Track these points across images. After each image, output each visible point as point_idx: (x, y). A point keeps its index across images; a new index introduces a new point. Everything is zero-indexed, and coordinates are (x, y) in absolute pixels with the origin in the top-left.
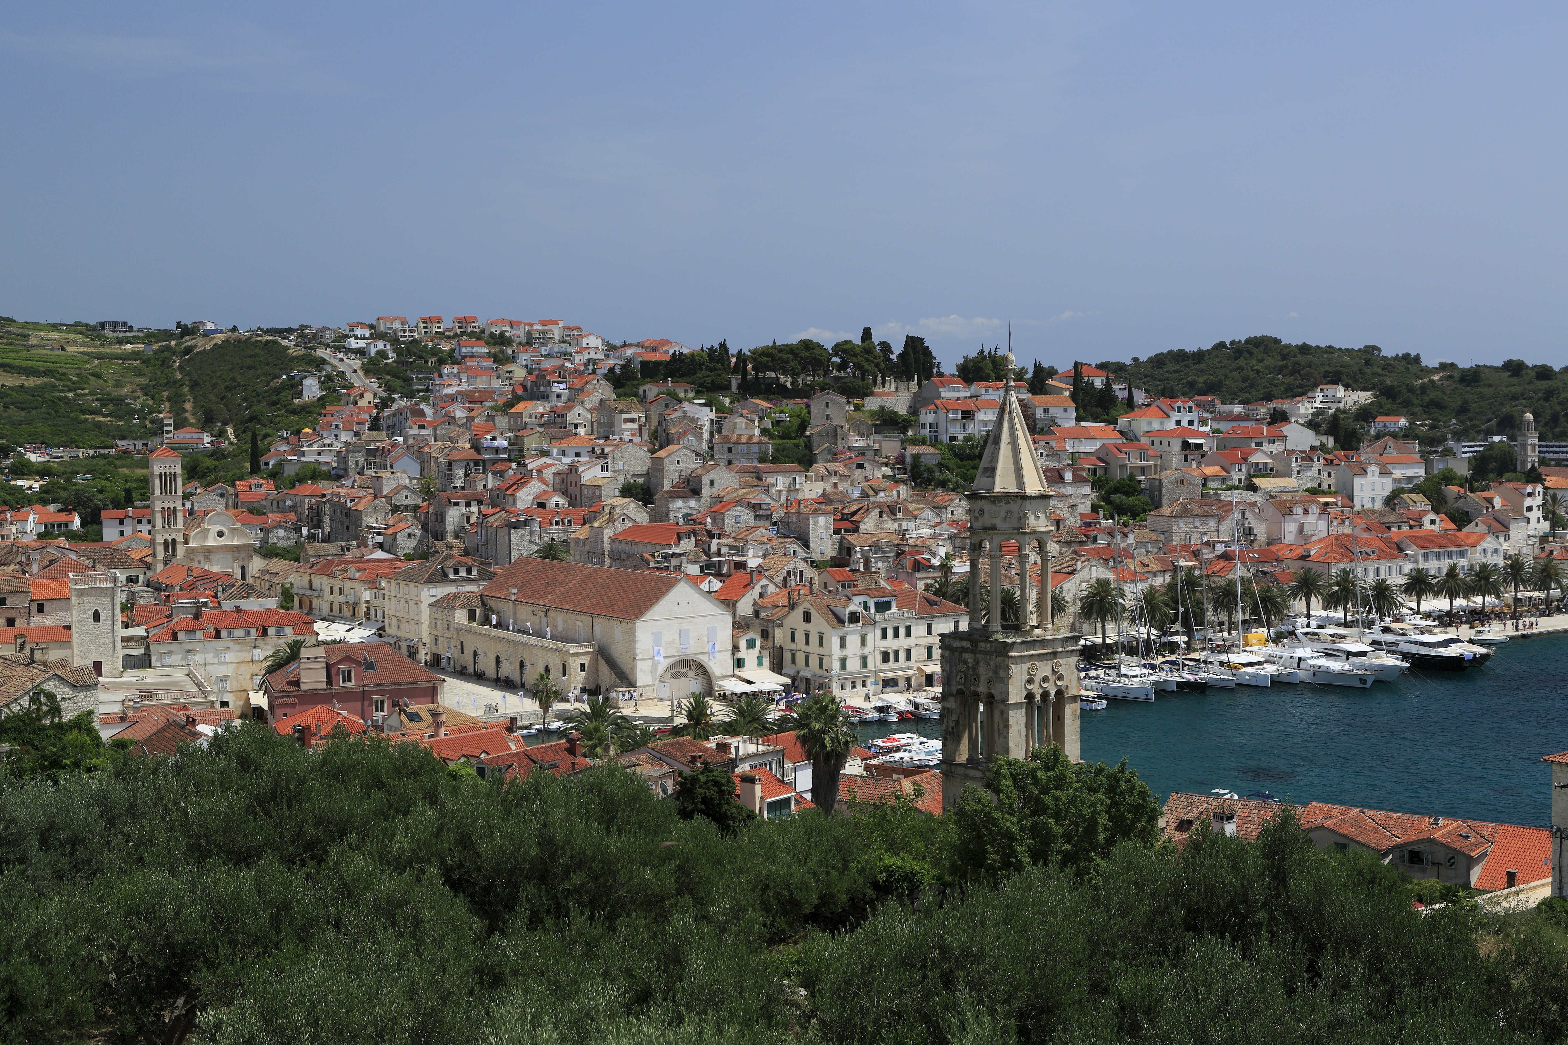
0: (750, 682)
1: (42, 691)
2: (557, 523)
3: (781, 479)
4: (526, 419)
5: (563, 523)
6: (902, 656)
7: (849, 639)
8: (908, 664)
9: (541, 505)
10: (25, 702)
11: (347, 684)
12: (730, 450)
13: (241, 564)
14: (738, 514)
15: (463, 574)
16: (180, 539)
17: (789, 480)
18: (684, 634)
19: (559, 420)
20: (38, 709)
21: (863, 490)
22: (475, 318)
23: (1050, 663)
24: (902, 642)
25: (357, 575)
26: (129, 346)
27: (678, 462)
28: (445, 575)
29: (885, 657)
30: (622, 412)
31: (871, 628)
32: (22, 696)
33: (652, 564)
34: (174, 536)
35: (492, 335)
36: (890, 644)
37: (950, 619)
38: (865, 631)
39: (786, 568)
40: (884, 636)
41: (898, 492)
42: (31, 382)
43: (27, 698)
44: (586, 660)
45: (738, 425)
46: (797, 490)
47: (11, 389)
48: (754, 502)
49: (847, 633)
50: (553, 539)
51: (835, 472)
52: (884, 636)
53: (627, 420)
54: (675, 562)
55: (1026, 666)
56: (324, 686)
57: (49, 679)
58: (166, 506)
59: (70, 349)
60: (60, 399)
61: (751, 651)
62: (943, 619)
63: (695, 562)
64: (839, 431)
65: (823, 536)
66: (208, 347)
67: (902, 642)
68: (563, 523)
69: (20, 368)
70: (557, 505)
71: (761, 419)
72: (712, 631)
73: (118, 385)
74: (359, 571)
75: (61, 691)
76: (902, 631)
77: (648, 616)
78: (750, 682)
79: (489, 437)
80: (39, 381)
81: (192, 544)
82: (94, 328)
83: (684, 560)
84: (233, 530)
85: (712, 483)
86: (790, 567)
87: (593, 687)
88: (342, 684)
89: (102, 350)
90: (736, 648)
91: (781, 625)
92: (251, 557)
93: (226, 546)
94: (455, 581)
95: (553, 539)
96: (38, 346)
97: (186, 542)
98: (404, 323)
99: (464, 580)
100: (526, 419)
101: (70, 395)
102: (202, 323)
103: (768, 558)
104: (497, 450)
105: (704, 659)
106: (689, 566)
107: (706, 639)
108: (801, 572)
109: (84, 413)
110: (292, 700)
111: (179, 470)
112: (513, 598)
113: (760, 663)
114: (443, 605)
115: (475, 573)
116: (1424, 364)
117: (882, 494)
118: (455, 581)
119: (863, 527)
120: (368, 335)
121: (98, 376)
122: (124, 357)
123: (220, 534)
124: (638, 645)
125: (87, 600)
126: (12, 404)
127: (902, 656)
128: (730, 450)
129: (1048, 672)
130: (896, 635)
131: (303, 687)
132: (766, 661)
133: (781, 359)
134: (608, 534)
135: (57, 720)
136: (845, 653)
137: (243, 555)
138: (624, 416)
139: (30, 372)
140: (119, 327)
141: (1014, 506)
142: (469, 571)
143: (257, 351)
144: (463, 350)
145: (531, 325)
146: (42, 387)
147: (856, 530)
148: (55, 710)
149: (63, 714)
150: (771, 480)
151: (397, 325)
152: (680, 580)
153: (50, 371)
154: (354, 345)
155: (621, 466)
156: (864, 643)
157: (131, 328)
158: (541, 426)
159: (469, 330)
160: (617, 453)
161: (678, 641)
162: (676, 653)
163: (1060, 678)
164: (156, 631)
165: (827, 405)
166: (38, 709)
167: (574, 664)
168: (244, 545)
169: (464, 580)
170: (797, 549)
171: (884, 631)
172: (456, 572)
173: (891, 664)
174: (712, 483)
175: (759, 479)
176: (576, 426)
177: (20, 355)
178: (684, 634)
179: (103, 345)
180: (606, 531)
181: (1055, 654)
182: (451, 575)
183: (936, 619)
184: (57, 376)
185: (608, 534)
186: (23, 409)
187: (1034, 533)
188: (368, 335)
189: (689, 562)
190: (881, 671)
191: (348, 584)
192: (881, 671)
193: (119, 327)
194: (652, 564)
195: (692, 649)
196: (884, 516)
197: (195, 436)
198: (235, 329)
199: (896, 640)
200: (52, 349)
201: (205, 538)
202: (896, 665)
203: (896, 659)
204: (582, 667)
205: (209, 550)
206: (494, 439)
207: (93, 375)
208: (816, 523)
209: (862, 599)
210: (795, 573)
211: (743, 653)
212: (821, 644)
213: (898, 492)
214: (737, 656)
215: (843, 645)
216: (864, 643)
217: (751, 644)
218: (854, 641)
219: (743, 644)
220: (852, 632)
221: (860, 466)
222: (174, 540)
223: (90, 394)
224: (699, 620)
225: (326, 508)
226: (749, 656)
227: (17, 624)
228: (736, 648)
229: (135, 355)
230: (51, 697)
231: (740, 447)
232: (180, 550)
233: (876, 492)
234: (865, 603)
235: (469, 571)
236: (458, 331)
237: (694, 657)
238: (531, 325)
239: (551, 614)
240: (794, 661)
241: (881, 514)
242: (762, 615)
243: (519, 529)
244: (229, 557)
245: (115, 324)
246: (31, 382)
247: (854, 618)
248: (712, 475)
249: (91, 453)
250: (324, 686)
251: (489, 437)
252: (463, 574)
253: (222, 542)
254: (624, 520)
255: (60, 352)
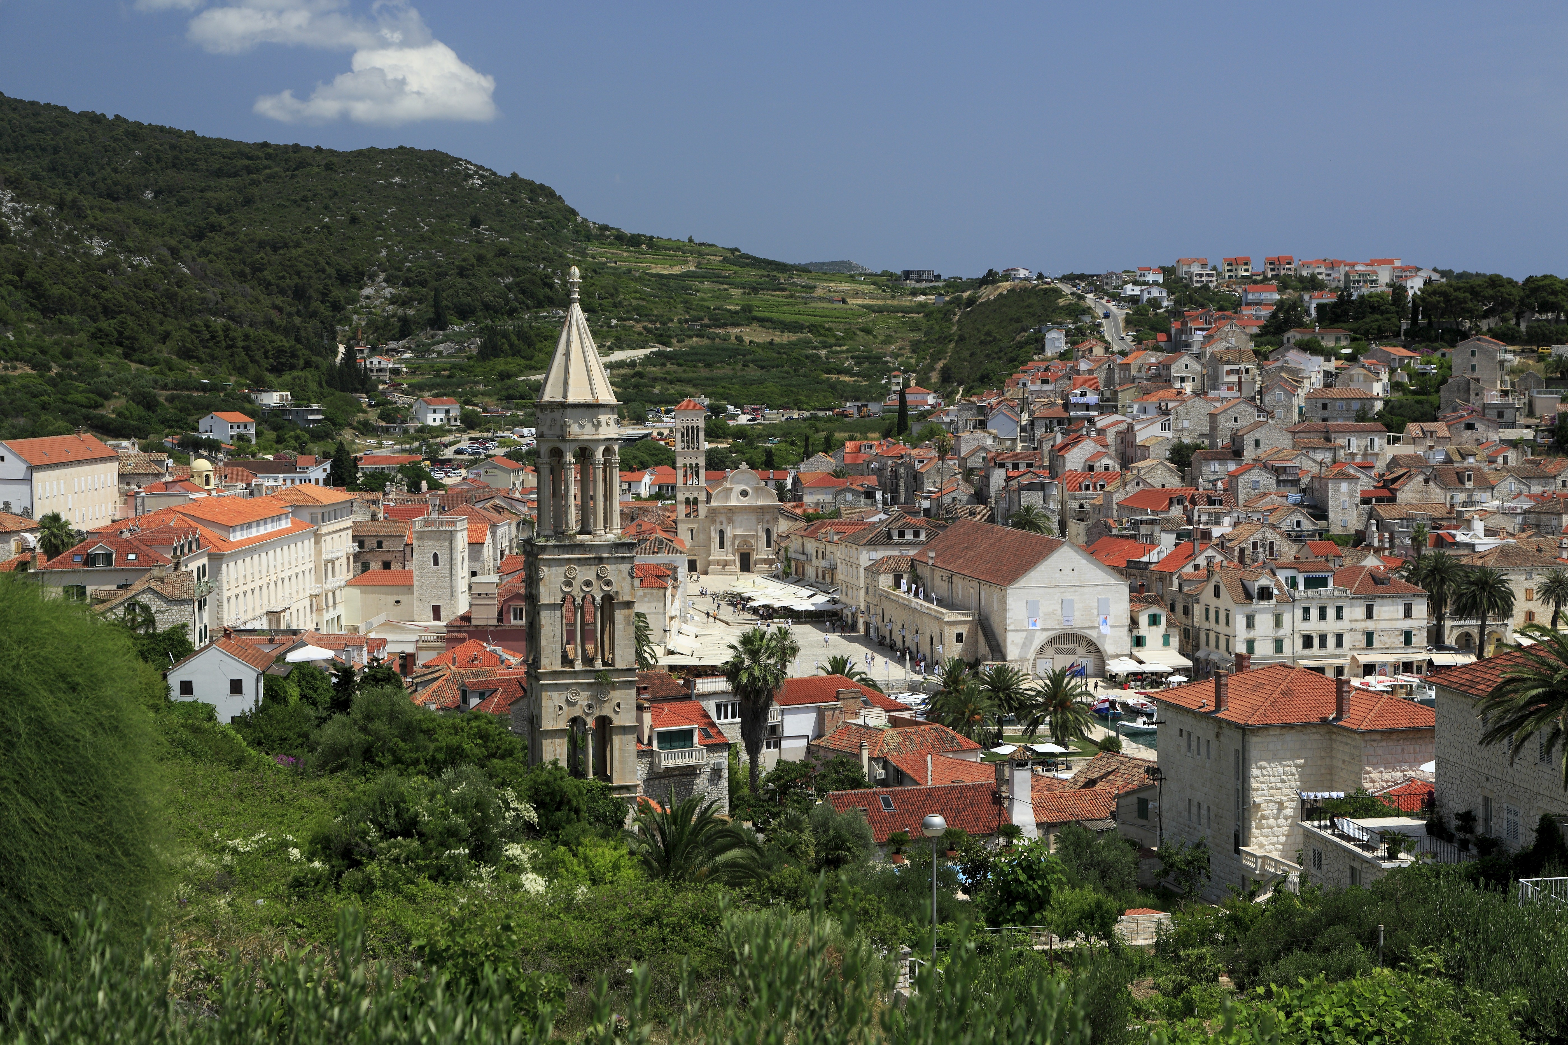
0: (1141, 662)
1: (137, 603)
2: (1087, 488)
3: (1355, 441)
4: (1134, 372)
5: (1095, 488)
6: (1331, 641)
7: (1258, 619)
8: (1339, 651)
9: (1091, 468)
10: (120, 612)
11: (518, 622)
12: (1325, 406)
13: (766, 526)
14: (1255, 478)
15: (909, 536)
16: (703, 497)
17: (1365, 442)
18: (1068, 605)
19: (1164, 372)
20: (133, 620)
21: (1447, 454)
22: (1291, 258)
23: (594, 568)
24: (1331, 625)
25: (836, 538)
26: (922, 298)
27: (1236, 419)
28: (889, 536)
29: (1308, 642)
30: (1228, 362)
31: (1288, 607)
32: (117, 606)
33: (1115, 532)
34: (695, 495)
35: (1301, 279)
36: (1314, 626)
37: (1399, 600)
38: (1280, 609)
39: (1252, 539)
40: (1306, 618)
41: (1506, 459)
42: (781, 338)
43: (122, 608)
44: (964, 630)
45: (1355, 378)
46: (1377, 454)
47: (758, 345)
48: (1278, 464)
49: (1256, 611)
50: (1081, 507)
51: (1432, 433)
52: (1306, 618)
53: (1230, 372)
54: (1144, 530)
55: (561, 570)
56: (495, 622)
57: (143, 592)
58: (688, 462)
59: (853, 302)
60: (807, 357)
61: (1154, 628)
62: (1389, 601)
63: (1171, 531)
64: (1472, 386)
65: (1346, 505)
66: (992, 297)
67: (1331, 625)
68: (1095, 488)
69: (782, 323)
70: (1107, 468)
71: (1392, 371)
72: (1103, 604)
73: (888, 340)
74: (837, 533)
75: (155, 605)
76: (1331, 613)
77: (1022, 582)
78: (1141, 662)
79: (1078, 391)
80: (794, 337)
81: (713, 504)
82: (898, 278)
83: (1157, 528)
84: (757, 490)
85: (1257, 443)
86: (1257, 537)
87: (972, 660)
88: (512, 622)
89: (889, 302)
90: (1134, 622)
91: (1198, 602)
92: (777, 520)
93: (750, 507)
94: (898, 544)
95: (1081, 507)
96: (821, 299)
97: (708, 502)
98: (1204, 266)
99: (909, 543)
100: (1134, 372)
101: (823, 352)
102: (1015, 270)
103: (1239, 527)
104: (1088, 407)
105: (1093, 634)
106: (1163, 535)
107: (1095, 612)
108: (1272, 544)
109: (829, 372)
110: (461, 635)
111: (702, 424)
112: (931, 562)
113: (1166, 643)
114: (873, 571)
115: (923, 536)
116: (1521, 282)
117: (1471, 460)
118: (898, 544)
119: (1400, 496)
120: (1161, 281)
121: (867, 331)
122: (905, 311)
123: (744, 493)
124: (1009, 615)
125: (427, 543)
126: (753, 361)
127: (1331, 641)
128: (1325, 406)
129: (592, 577)
130: (1323, 616)
131: (474, 622)
132: (1175, 641)
133: (1456, 298)
134: (1117, 498)
135: (151, 631)
136: (1252, 634)
137: (768, 517)
138: (1227, 367)
139: (795, 327)
140: (925, 277)
141: (557, 414)
142: (916, 534)
143: (1033, 300)
144: (1250, 297)
145: (1353, 265)
146: (792, 345)
147: (1393, 500)
148: (150, 621)
149: (158, 625)
150: (1342, 441)
151: (1196, 269)
152: (1063, 543)
153: (814, 326)
154: (1129, 293)
155: (1186, 424)
156: (1278, 624)
157: (938, 277)
158: (1148, 379)
159: (1283, 272)
160: (1180, 409)
161: (1059, 612)
162: (1057, 625)
163: (608, 583)
164: (509, 578)
165: (1473, 354)
166: (133, 620)
167: (950, 633)
168: (769, 507)
169: (909, 543)
170: (1301, 519)
171: (1306, 610)
172: (902, 534)
173: (1316, 649)
174: (1257, 443)
175: (1328, 440)
176: (1182, 380)
177: (796, 308)
178: (1068, 605)
179: (893, 297)
180: (1115, 497)
181: (600, 560)
182: (896, 538)
183: (1379, 601)
184: (822, 331)
185: (1117, 498)
186: (762, 368)
187: (577, 441)
188: (1161, 281)
189: (1164, 530)
190: (1302, 658)
191: (829, 548)
192: (1302, 658)
193: (925, 277)
194: (1115, 532)
195: (1078, 622)
196: (1431, 483)
197: (919, 397)
198: (1040, 277)
199: (1323, 623)
200: (833, 302)
201: (728, 498)
202: (1323, 652)
203: (1323, 644)
204: (959, 638)
205: (732, 511)
206: (1084, 394)
207: (862, 330)
208: (1337, 491)
209: (1290, 573)
210: (1263, 545)
211: (1144, 629)
212: (1227, 623)
213: (1506, 459)
214: (1135, 633)
215: (1250, 624)
216: (1278, 624)
217: (1154, 620)
218: (1264, 622)
219: (1143, 620)
220: (1263, 611)
221: (1470, 427)
222: (696, 499)
223: (848, 351)
224: (1086, 590)
225: (902, 470)
226: (1153, 635)
227: (393, 566)
228: (1134, 622)
229: (923, 306)
230: (146, 609)
231: (1338, 403)
232: (703, 509)
233: (1463, 457)
234: (1294, 579)
235: (916, 534)
236: (1269, 274)
237: (1079, 632)
238: (1353, 265)
239: (955, 579)
240: (1207, 644)
241: (1426, 481)
242: (1185, 589)
243: (1030, 493)
244: (753, 518)
245: (921, 273)
246: (781, 338)
247: (1265, 594)
248: (1257, 434)
249: (806, 414)
250: (495, 622)
251: (1078, 391)
252: (909, 536)
253: (745, 502)
254: (1138, 484)
255: (841, 305)
